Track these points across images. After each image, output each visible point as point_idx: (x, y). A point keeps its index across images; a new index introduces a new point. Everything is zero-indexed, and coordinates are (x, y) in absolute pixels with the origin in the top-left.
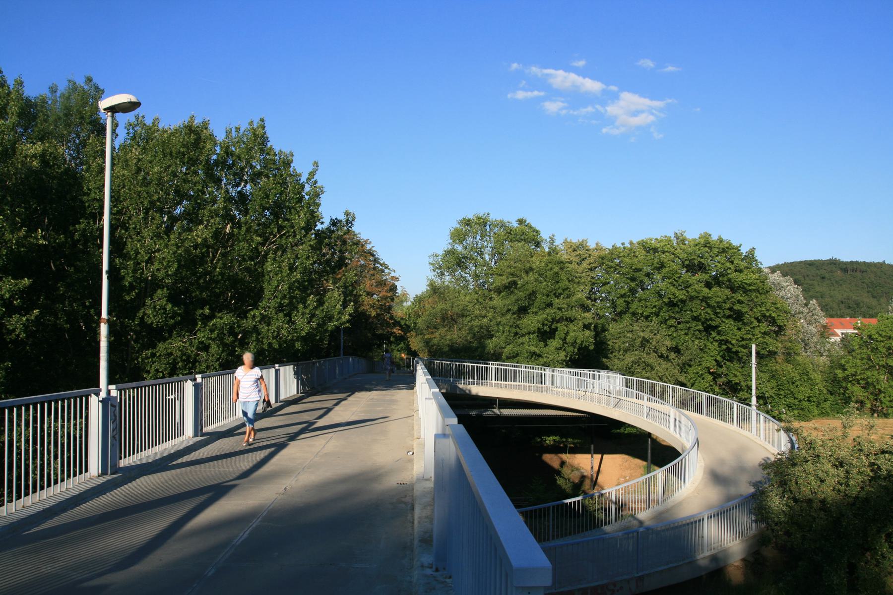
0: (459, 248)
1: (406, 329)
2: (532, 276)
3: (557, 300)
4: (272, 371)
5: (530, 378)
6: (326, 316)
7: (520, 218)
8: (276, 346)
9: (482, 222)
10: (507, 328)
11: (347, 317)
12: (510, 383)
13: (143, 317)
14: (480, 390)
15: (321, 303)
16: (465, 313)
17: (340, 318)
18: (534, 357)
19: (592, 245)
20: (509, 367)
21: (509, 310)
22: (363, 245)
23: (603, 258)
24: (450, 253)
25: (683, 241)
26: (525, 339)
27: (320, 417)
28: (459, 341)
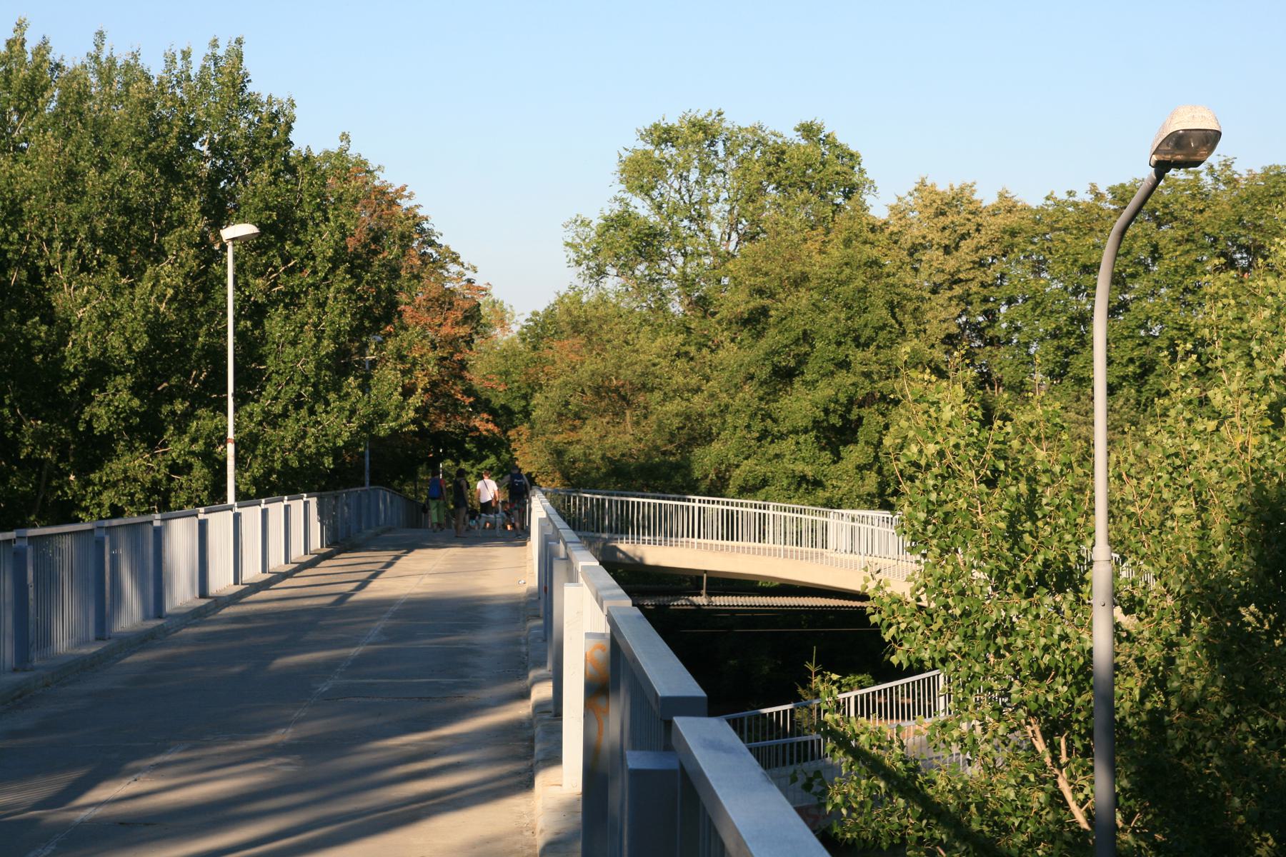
0: (641, 207)
1: (504, 416)
2: (803, 298)
3: (860, 355)
4: (301, 503)
5: (730, 528)
6: (375, 413)
7: (807, 119)
8: (296, 464)
9: (704, 131)
10: (743, 420)
11: (412, 414)
12: (746, 544)
13: (91, 420)
14: (656, 554)
15: (365, 387)
16: (650, 381)
17: (398, 416)
18: (806, 486)
20: (746, 508)
21: (752, 377)
22: (392, 203)
23: (1013, 234)
24: (620, 221)
25: (1231, 182)
26: (787, 446)
27: (359, 589)
28: (635, 447)
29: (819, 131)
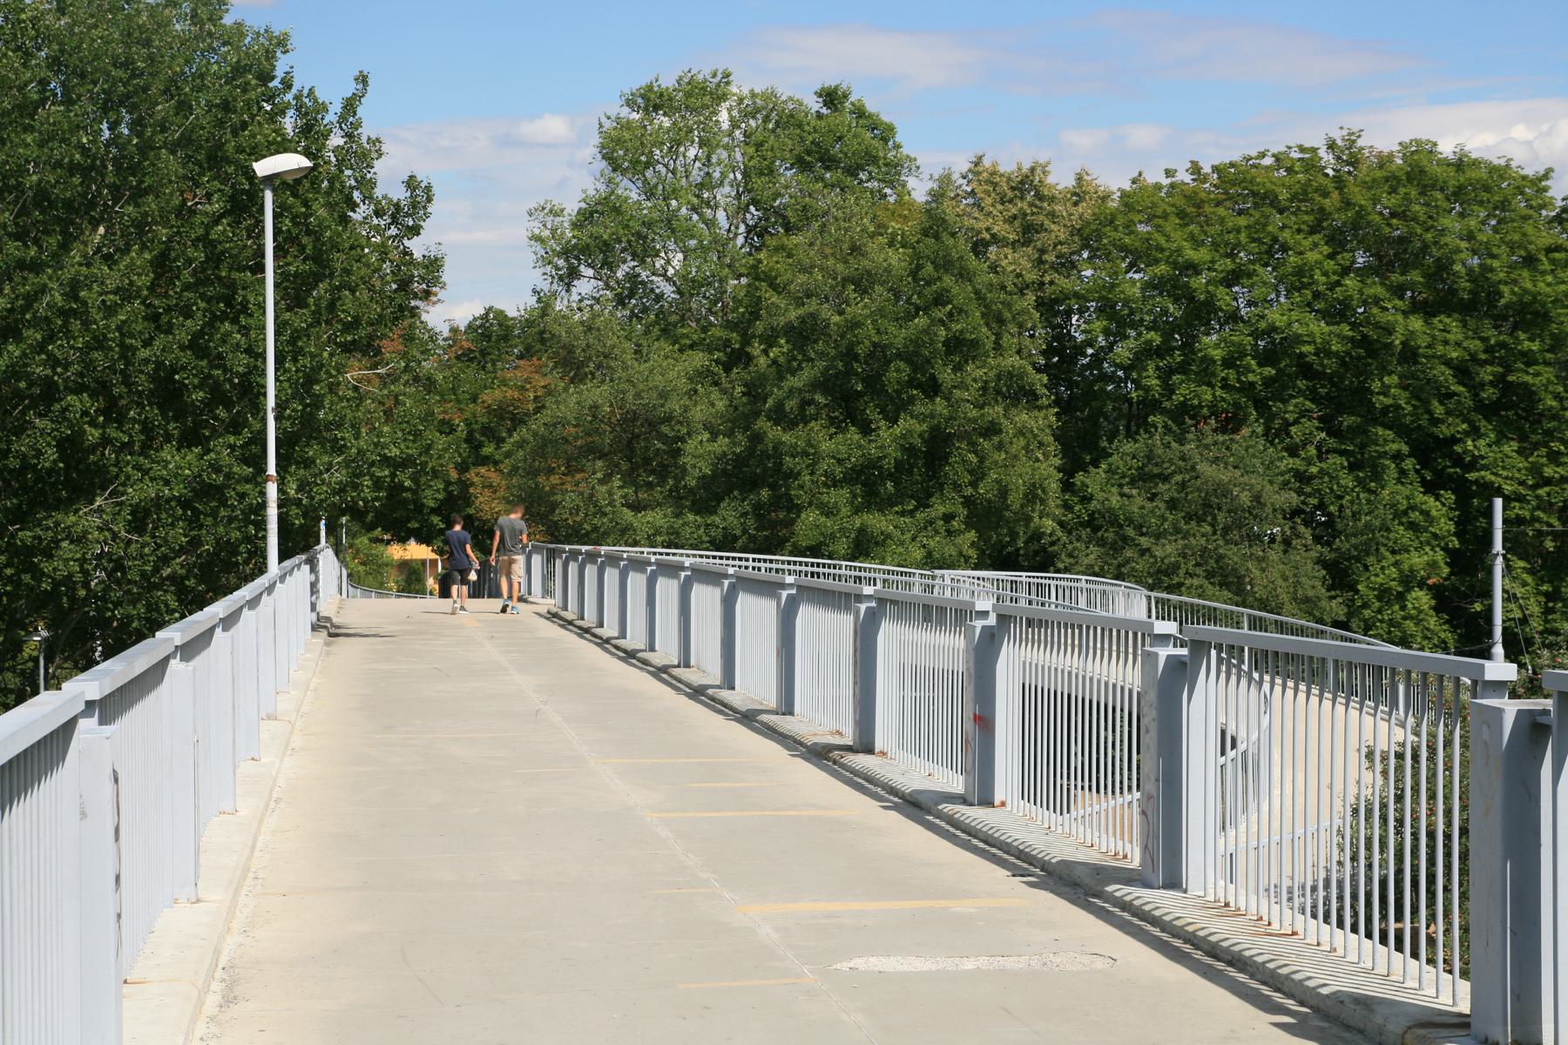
0: (630, 191)
7: (831, 82)
9: (700, 96)
19: (1061, 179)
29: (845, 96)
